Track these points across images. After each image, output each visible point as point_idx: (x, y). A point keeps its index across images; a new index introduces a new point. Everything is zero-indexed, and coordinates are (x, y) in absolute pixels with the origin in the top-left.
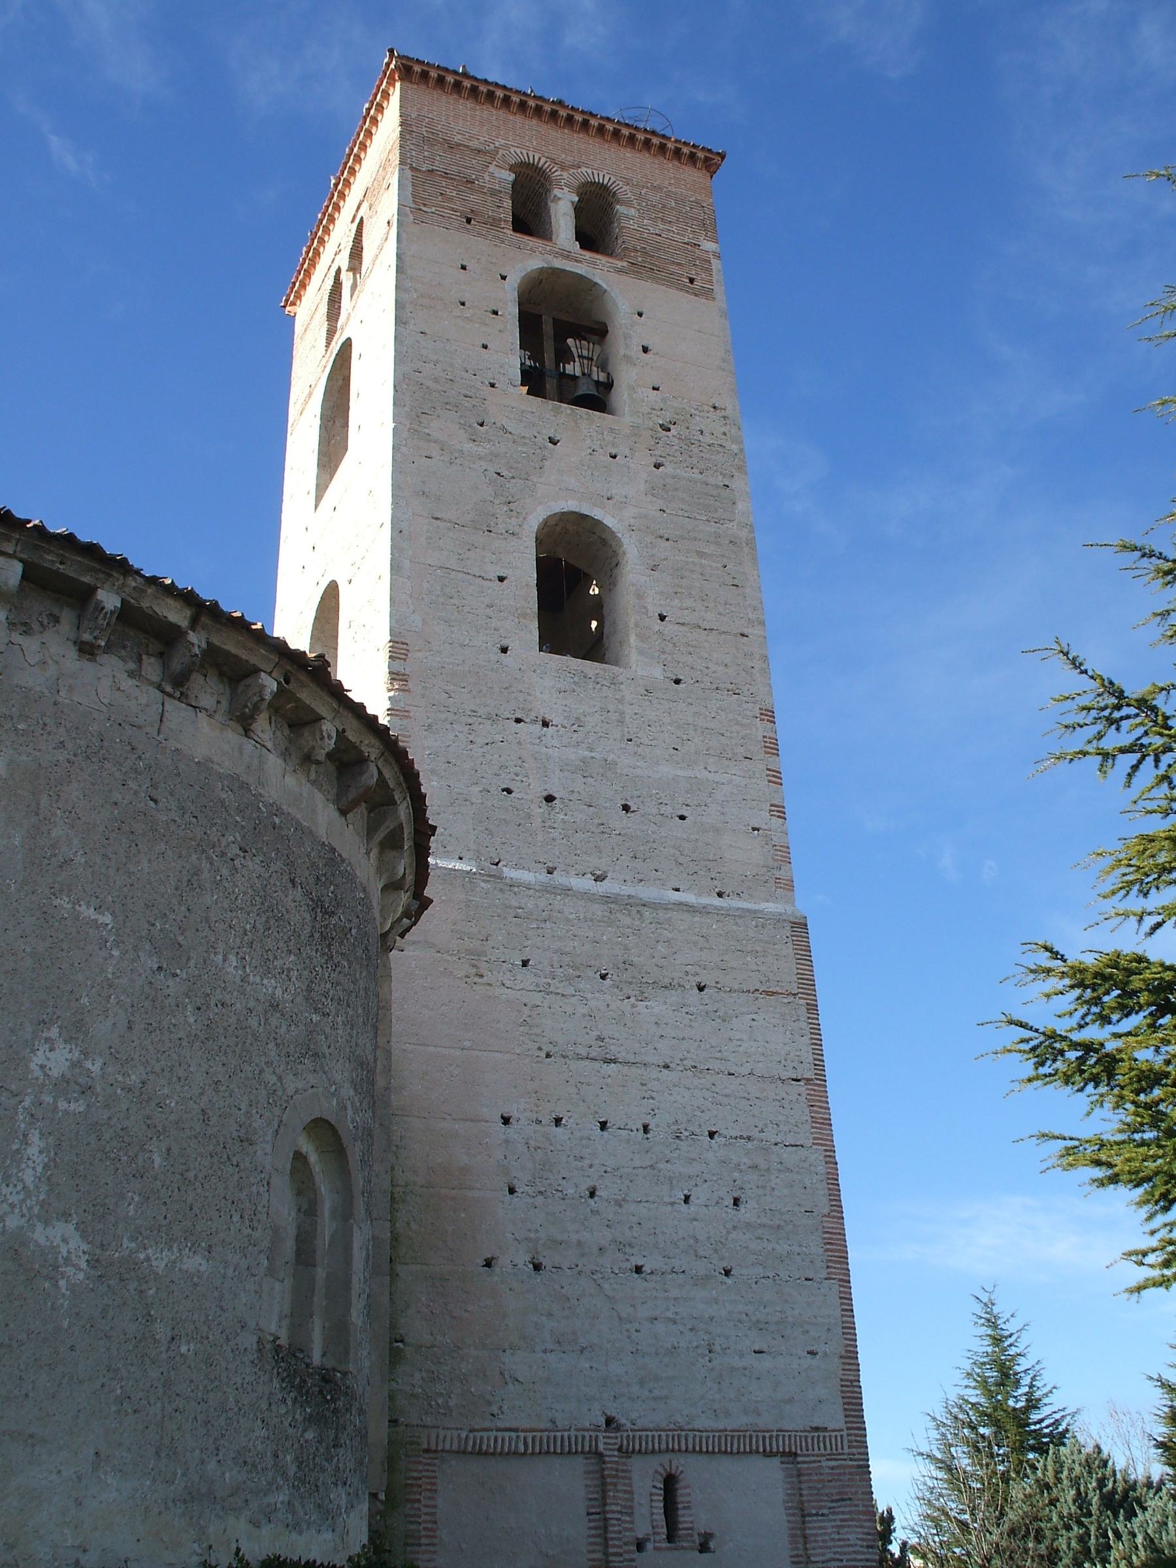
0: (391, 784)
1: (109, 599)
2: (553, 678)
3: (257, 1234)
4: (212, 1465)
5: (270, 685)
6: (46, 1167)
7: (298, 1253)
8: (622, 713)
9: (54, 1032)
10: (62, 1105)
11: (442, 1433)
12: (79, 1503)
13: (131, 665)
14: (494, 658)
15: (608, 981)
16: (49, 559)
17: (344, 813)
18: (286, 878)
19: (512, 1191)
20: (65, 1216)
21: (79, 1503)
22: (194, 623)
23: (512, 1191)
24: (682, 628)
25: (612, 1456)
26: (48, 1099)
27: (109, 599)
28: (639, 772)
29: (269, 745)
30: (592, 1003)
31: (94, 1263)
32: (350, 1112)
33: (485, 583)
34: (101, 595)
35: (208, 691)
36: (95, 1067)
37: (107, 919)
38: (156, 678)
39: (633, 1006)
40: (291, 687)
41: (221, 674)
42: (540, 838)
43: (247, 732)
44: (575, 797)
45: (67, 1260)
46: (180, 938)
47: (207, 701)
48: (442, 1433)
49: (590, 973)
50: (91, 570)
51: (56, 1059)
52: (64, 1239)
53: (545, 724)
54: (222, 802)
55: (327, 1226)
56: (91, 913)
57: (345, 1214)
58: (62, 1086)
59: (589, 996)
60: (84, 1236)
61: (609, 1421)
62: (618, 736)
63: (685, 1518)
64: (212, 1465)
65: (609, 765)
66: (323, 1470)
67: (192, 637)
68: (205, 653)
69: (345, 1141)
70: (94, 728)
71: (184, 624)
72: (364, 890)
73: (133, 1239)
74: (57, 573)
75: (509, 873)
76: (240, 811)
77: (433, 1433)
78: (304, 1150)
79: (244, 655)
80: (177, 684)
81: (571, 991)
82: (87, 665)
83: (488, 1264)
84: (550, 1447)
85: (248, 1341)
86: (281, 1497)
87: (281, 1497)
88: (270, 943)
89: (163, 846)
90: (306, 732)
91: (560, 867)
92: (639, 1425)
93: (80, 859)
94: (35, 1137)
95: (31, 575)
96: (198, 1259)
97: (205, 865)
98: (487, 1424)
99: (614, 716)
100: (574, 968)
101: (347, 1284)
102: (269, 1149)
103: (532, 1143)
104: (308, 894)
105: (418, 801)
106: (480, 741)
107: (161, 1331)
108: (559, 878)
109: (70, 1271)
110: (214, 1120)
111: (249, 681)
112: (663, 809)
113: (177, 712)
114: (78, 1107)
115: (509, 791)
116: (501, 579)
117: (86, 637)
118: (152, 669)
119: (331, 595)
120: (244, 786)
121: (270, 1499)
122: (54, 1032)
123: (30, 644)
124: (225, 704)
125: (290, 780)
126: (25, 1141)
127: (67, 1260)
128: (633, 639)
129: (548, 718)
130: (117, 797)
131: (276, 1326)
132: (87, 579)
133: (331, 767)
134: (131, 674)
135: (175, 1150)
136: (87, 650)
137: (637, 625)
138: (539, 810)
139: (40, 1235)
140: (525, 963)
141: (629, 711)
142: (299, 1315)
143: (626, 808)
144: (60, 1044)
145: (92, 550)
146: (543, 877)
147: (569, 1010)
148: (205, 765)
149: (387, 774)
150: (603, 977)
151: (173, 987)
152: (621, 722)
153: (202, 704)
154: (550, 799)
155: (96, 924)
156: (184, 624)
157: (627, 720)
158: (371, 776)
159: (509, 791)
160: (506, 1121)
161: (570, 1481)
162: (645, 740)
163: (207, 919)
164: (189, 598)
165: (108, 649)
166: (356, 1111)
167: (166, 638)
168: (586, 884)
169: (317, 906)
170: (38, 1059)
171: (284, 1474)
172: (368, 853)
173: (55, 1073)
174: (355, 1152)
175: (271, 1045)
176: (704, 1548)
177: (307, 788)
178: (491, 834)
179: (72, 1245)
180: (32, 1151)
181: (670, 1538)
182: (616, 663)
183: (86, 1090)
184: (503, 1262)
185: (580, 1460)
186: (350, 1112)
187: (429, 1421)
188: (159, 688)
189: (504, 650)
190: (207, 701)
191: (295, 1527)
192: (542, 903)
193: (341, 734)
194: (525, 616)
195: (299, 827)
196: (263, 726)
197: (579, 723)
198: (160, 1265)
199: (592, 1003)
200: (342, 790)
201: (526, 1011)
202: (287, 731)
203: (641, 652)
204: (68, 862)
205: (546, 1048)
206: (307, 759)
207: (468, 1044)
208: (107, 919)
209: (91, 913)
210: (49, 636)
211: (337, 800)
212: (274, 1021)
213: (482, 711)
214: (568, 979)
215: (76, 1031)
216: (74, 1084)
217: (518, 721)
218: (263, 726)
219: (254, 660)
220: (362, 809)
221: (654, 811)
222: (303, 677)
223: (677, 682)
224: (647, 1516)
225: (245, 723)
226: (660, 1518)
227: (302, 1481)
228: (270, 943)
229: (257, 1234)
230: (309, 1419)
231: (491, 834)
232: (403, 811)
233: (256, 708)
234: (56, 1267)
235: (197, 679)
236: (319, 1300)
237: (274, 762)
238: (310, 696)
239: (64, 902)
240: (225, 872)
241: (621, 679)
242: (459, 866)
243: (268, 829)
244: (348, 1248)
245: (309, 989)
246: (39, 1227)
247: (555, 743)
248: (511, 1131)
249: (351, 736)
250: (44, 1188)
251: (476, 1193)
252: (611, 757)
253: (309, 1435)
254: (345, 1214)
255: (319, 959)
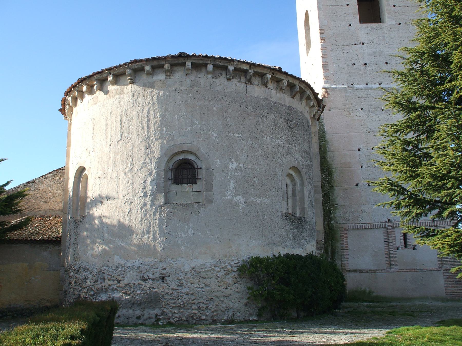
0: (303, 88)
1: (231, 68)
2: (365, 31)
3: (279, 193)
4: (273, 238)
5: (269, 76)
6: (234, 186)
7: (293, 194)
8: (384, 37)
9: (233, 160)
10: (236, 174)
11: (348, 225)
12: (248, 245)
13: (239, 80)
14: (347, 28)
15: (384, 111)
16: (218, 63)
17: (293, 97)
18: (279, 117)
19: (362, 167)
20: (239, 195)
21: (248, 245)
22: (250, 68)
23: (362, 167)
24: (401, 8)
25: (390, 228)
26: (233, 173)
27: (231, 68)
28: (389, 52)
29: (272, 88)
30: (380, 117)
31: (246, 203)
32: (301, 163)
33: (343, 7)
34: (229, 67)
35: (256, 81)
36: (242, 166)
37: (240, 135)
38: (244, 81)
39: (391, 117)
40: (275, 75)
41: (259, 76)
42: (364, 75)
43: (266, 87)
44: (372, 63)
45: (241, 203)
46: (256, 136)
47: (256, 83)
48: (348, 225)
49: (379, 109)
50: (226, 63)
51: (234, 165)
52: (240, 199)
53: (363, 44)
54: (262, 104)
55: (298, 187)
56: (237, 135)
57: (302, 185)
58: (235, 170)
59: (379, 115)
60: (243, 198)
61: (389, 220)
62: (383, 43)
63: (409, 242)
64: (273, 238)
65: (381, 52)
66: (299, 237)
67: (250, 71)
68: (253, 74)
69: (300, 170)
70: (233, 96)
71: (248, 68)
72: (301, 113)
73: (253, 197)
74: (220, 65)
75: (356, 86)
76: (266, 105)
77: (346, 225)
78: (291, 173)
79: (262, 71)
80: (249, 81)
81: (374, 115)
82: (229, 82)
83: (357, 185)
84: (374, 227)
85: (280, 214)
86: (289, 243)
87: (289, 243)
88: (277, 132)
89: (250, 118)
90: (280, 83)
91: (370, 82)
92: (396, 220)
93: (234, 124)
94: (232, 181)
95: (214, 66)
96: (267, 199)
97: (260, 119)
98: (359, 222)
99: (382, 38)
100: (375, 109)
101: (304, 199)
102: (280, 175)
103: (366, 155)
104: (285, 119)
105: (312, 90)
106: (346, 52)
107: (260, 214)
108: (369, 85)
109: (241, 205)
110: (267, 172)
111: (264, 76)
112: (397, 62)
113: (250, 87)
114: (239, 174)
115: (354, 64)
116: (348, 5)
117: (228, 77)
118: (243, 79)
119: (307, 13)
120: (267, 99)
121: (287, 243)
122: (233, 160)
123: (217, 81)
124: (260, 82)
125: (278, 95)
126: (230, 182)
127: (241, 203)
128: (386, 14)
129: (363, 42)
130: (239, 109)
131: (285, 211)
132: (226, 65)
133: (288, 88)
134: (239, 82)
135: (260, 179)
136: (229, 79)
137: (387, 10)
138: (363, 68)
139: (235, 199)
140: (362, 109)
141: (386, 35)
142: (294, 207)
143: (387, 63)
144: (234, 162)
145: (226, 59)
146: (365, 86)
147: (374, 120)
148: (257, 97)
149: (302, 86)
150: (382, 110)
151: (256, 146)
152: (384, 39)
153: (255, 84)
154: (365, 64)
155: (238, 137)
156: (248, 68)
157: (386, 38)
158: (298, 88)
159: (354, 64)
160: (359, 150)
161: (380, 234)
162: (391, 43)
163: (262, 131)
164: (247, 63)
165: (233, 77)
166: (303, 162)
167: (245, 72)
168: (377, 86)
169: (288, 121)
170: (230, 166)
171: (290, 239)
172: (301, 104)
173: (234, 168)
174: (303, 172)
175: (279, 154)
176: (414, 249)
177: (282, 95)
178: (351, 76)
179: (241, 200)
180: (232, 184)
181: (406, 246)
182: (383, 23)
183: (240, 170)
184: (360, 184)
185: (382, 229)
186: (301, 163)
187: (345, 222)
188: (246, 83)
189: (350, 25)
190: (256, 83)
191: (293, 248)
192: (365, 93)
193: (288, 82)
194: (355, 14)
195: (281, 104)
196: (270, 85)
197: (372, 42)
198: (259, 202)
199: (380, 117)
200: (292, 92)
201: (363, 121)
202: (276, 84)
203: (389, 18)
204: (231, 125)
205: (368, 131)
206: (281, 89)
207: (348, 132)
208: (240, 135)
209: (237, 135)
210: (221, 77)
211: (291, 95)
212: (279, 149)
213: (345, 44)
214: (373, 112)
215: (237, 159)
216: (238, 169)
217: (355, 44)
218: (270, 85)
219: (264, 72)
220: (299, 94)
221: (394, 63)
222: (277, 72)
223: (400, 24)
224: (399, 242)
225: (266, 85)
226: (403, 242)
227: (294, 240)
228: (277, 132)
229: (279, 193)
230: (295, 228)
231: (351, 76)
232: (309, 92)
233: (267, 82)
234: (239, 204)
235: (253, 79)
236: (298, 203)
237: (274, 92)
238: (279, 76)
239: (231, 134)
240: (265, 119)
241: (383, 27)
242: (343, 86)
243: (273, 107)
244: (303, 192)
245: (287, 140)
246: (235, 197)
247: (366, 49)
248: (360, 152)
249: (291, 81)
250: (235, 190)
251: (353, 168)
252: (382, 50)
253: (295, 231)
254: (302, 185)
255: (289, 132)
